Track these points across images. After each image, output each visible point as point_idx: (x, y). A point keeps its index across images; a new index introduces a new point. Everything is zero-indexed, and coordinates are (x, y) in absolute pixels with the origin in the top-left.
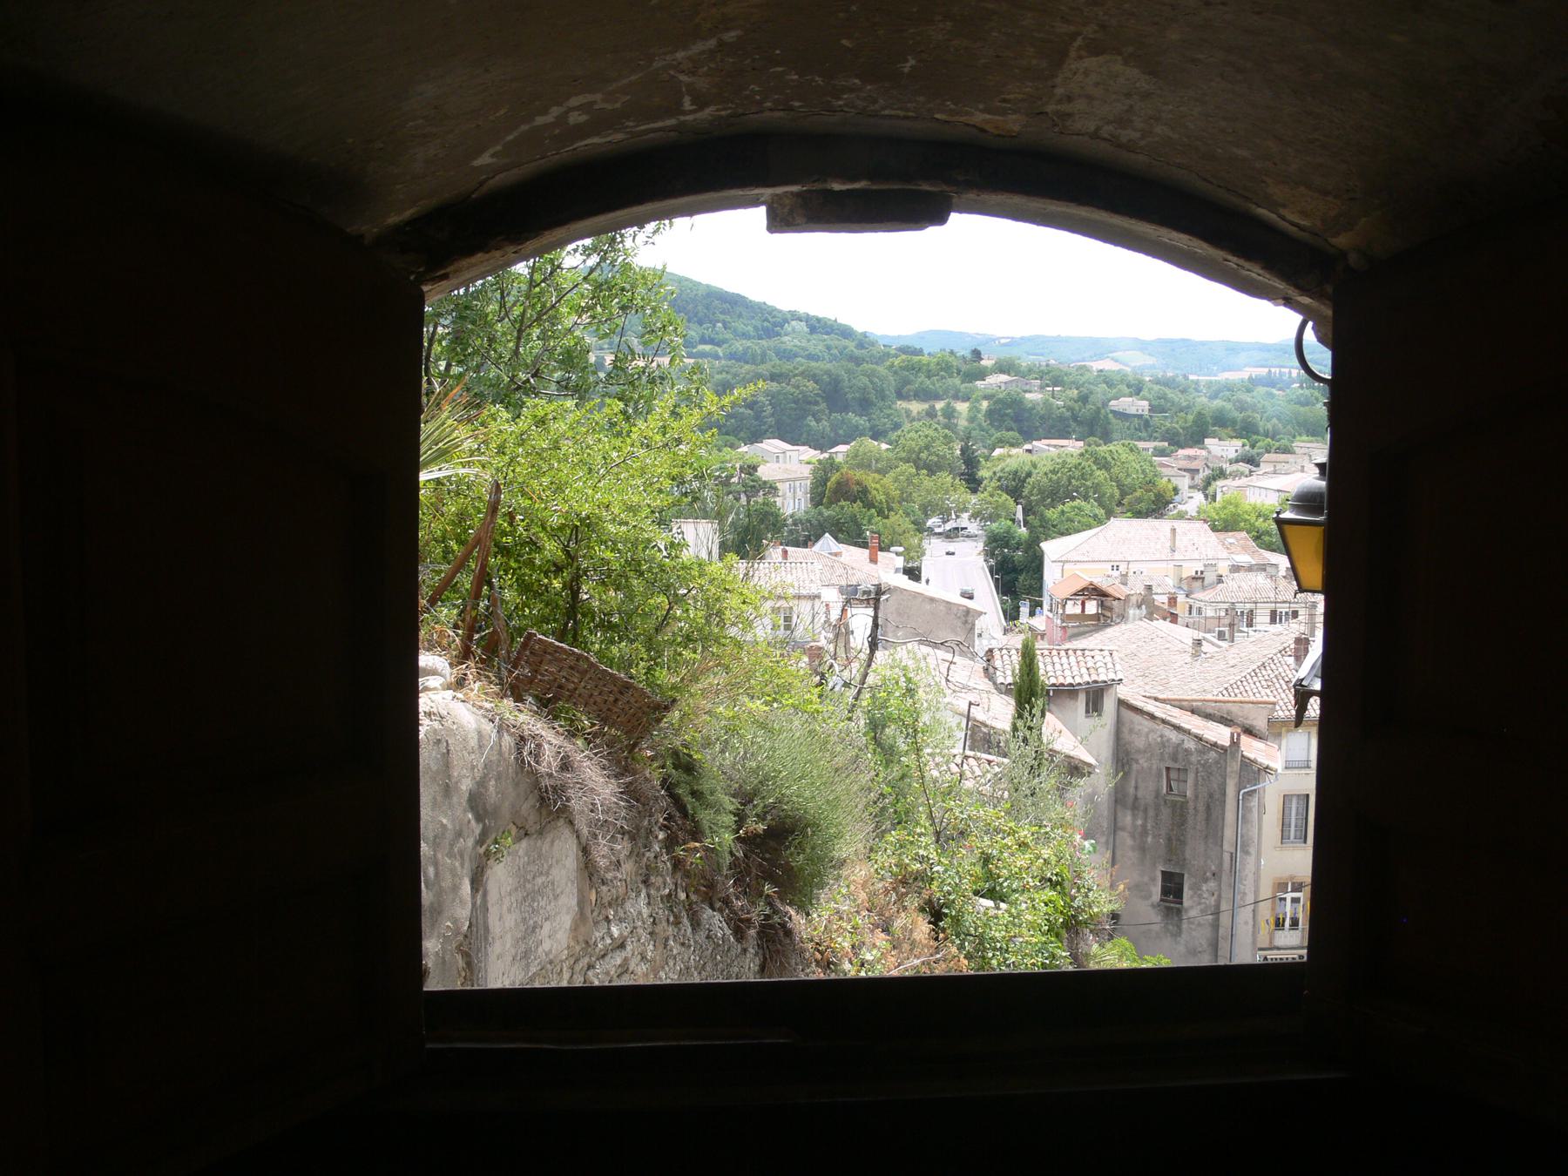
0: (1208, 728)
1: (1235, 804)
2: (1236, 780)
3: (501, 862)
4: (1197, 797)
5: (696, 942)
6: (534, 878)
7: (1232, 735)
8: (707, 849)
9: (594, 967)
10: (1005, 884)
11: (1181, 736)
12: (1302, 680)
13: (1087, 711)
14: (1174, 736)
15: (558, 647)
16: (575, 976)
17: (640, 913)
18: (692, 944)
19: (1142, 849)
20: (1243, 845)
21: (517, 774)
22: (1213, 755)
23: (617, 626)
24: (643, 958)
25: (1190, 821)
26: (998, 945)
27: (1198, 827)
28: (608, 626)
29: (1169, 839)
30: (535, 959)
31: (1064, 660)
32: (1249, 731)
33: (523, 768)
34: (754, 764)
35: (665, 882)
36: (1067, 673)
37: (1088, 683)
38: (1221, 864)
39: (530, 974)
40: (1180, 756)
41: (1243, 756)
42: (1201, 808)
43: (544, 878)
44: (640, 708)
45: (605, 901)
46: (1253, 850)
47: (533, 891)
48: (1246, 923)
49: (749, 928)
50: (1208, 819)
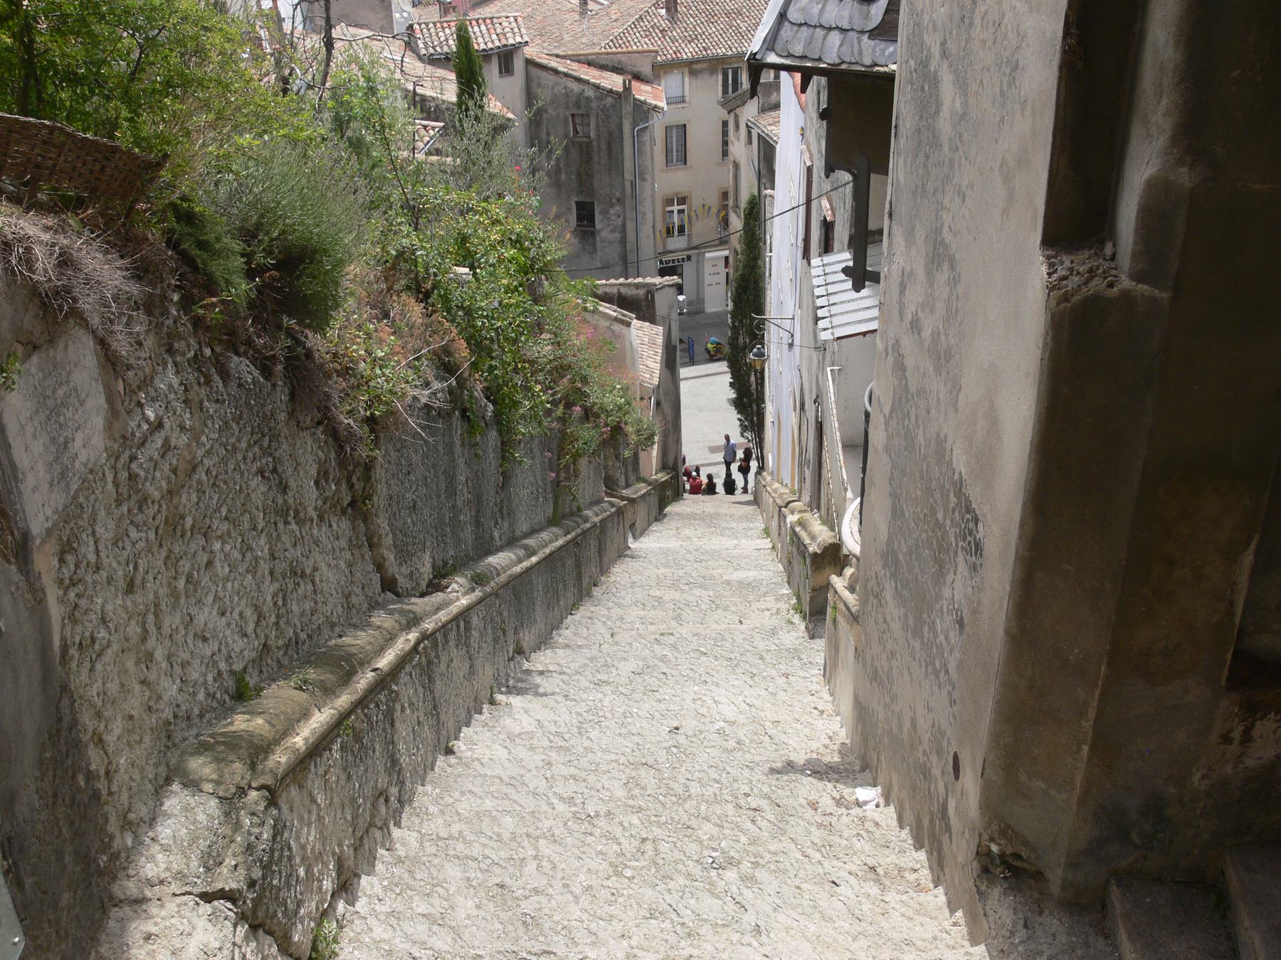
0: (604, 78)
1: (631, 140)
2: (631, 119)
3: (13, 390)
4: (599, 137)
5: (229, 395)
6: (54, 392)
7: (624, 81)
8: (223, 302)
9: (136, 458)
10: (483, 260)
11: (582, 87)
12: (756, 54)
13: (501, 72)
14: (575, 87)
15: (25, 122)
16: (119, 475)
17: (171, 386)
18: (225, 397)
19: (557, 185)
20: (640, 174)
21: (9, 286)
22: (609, 99)
23: (85, 77)
24: (181, 429)
25: (596, 157)
26: (485, 314)
27: (603, 162)
28: (73, 79)
29: (579, 175)
30: (74, 475)
31: (476, 29)
32: (638, 77)
33: (15, 281)
34: (251, 197)
35: (188, 346)
36: (480, 40)
37: (499, 47)
38: (623, 191)
39: (72, 493)
40: (582, 103)
41: (634, 99)
42: (604, 146)
43: (65, 388)
44: (130, 171)
45: (134, 387)
46: (648, 177)
47: (57, 406)
48: (648, 237)
49: (274, 364)
50: (609, 155)
